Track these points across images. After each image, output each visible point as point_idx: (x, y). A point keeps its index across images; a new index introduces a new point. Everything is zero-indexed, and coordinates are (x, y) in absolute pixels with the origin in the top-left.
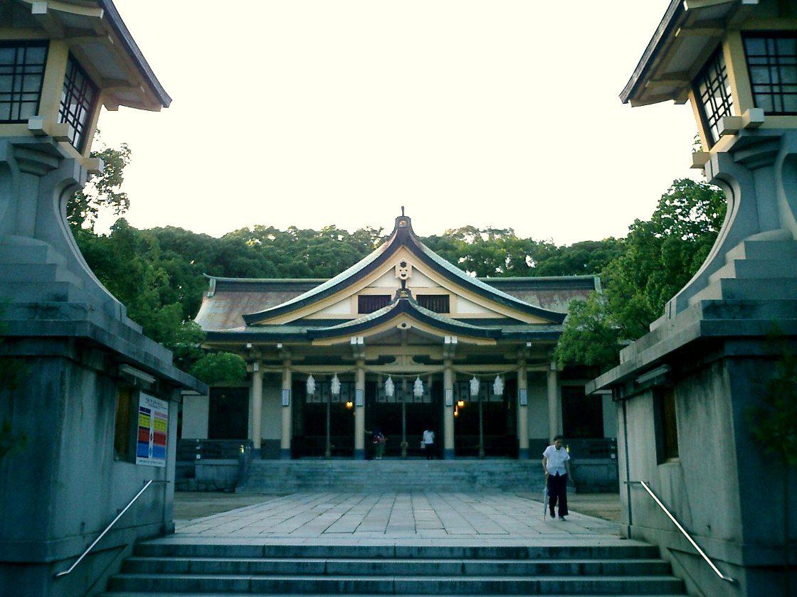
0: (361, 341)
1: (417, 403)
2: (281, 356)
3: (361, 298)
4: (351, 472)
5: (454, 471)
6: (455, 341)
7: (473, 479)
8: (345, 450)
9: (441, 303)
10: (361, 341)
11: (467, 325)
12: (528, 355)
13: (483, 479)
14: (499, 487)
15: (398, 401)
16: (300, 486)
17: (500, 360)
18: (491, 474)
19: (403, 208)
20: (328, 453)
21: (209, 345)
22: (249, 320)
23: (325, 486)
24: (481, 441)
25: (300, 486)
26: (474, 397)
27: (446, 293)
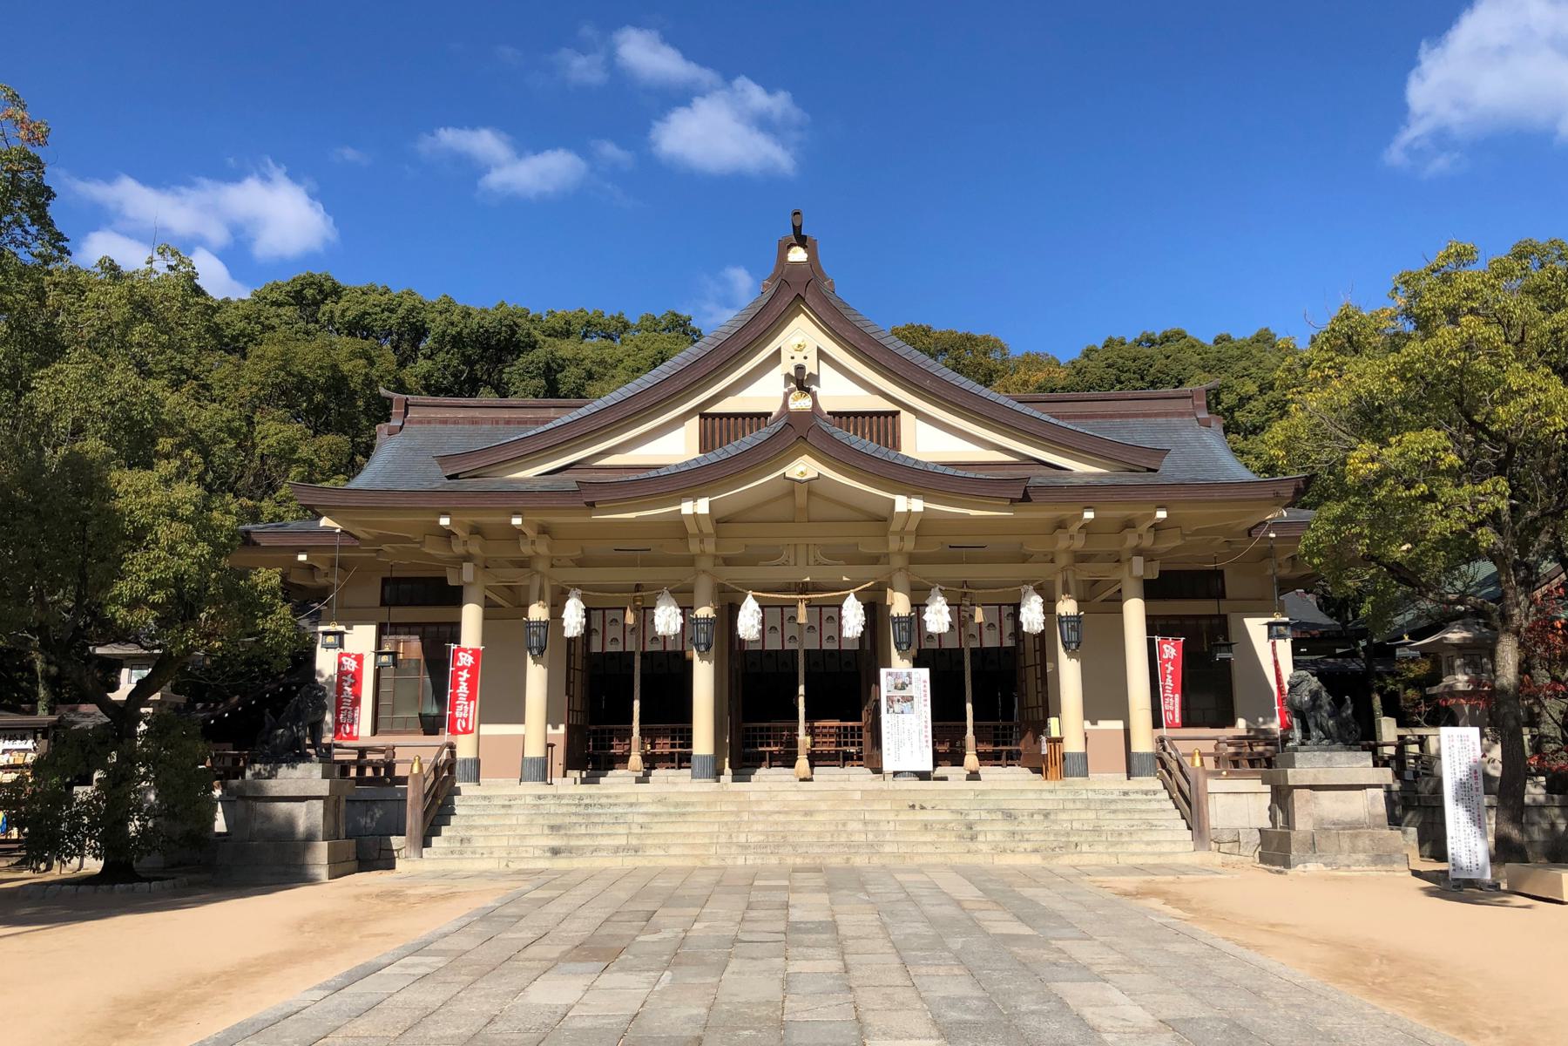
5: (922, 808)
9: (884, 424)
26: (852, 640)
27: (892, 407)
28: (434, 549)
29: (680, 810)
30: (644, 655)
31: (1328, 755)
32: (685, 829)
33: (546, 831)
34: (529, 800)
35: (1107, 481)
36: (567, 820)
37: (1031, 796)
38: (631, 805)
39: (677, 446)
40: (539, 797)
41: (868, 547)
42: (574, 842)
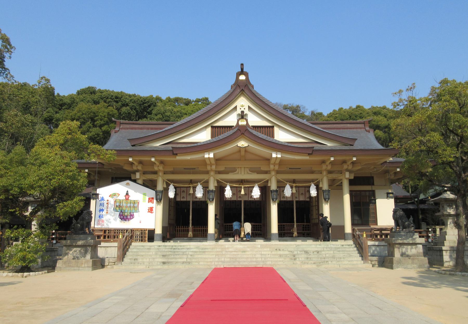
1: (250, 201)
2: (156, 168)
4: (204, 251)
5: (279, 250)
8: (201, 233)
15: (239, 199)
19: (242, 65)
22: (134, 142)
24: (295, 226)
28: (127, 168)
29: (204, 251)
30: (297, 202)
32: (205, 256)
33: (161, 257)
35: (338, 149)
36: (168, 253)
37: (313, 246)
38: (188, 249)
39: (203, 136)
40: (159, 246)
41: (264, 168)
42: (170, 260)
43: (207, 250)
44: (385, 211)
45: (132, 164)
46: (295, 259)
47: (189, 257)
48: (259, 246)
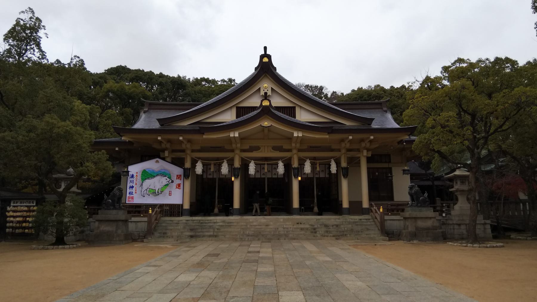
0: (237, 135)
3: (238, 108)
4: (229, 225)
6: (300, 135)
7: (314, 231)
8: (227, 210)
9: (291, 111)
10: (237, 135)
11: (310, 124)
12: (348, 145)
13: (322, 230)
14: (334, 236)
15: (263, 176)
16: (192, 237)
17: (330, 149)
18: (326, 226)
19: (265, 48)
20: (216, 210)
21: (132, 138)
23: (210, 236)
25: (192, 237)
31: (420, 208)
34: (184, 221)
37: (333, 220)
38: (215, 223)
40: (187, 220)
43: (232, 224)
44: (402, 187)
45: (160, 142)
46: (315, 233)
47: (216, 230)
48: (282, 220)
